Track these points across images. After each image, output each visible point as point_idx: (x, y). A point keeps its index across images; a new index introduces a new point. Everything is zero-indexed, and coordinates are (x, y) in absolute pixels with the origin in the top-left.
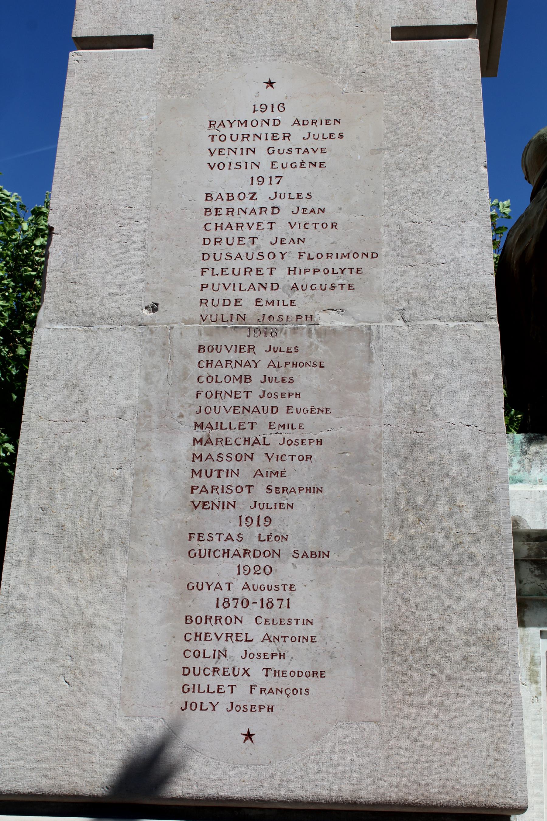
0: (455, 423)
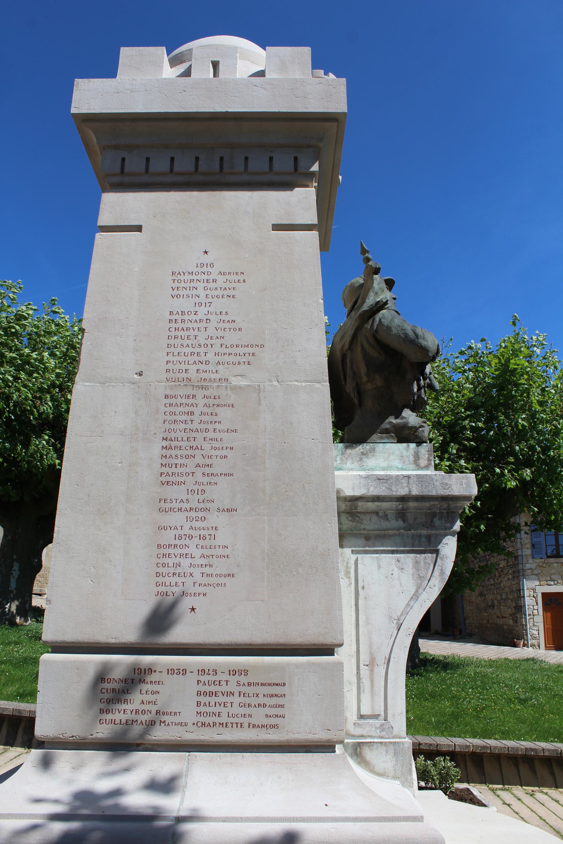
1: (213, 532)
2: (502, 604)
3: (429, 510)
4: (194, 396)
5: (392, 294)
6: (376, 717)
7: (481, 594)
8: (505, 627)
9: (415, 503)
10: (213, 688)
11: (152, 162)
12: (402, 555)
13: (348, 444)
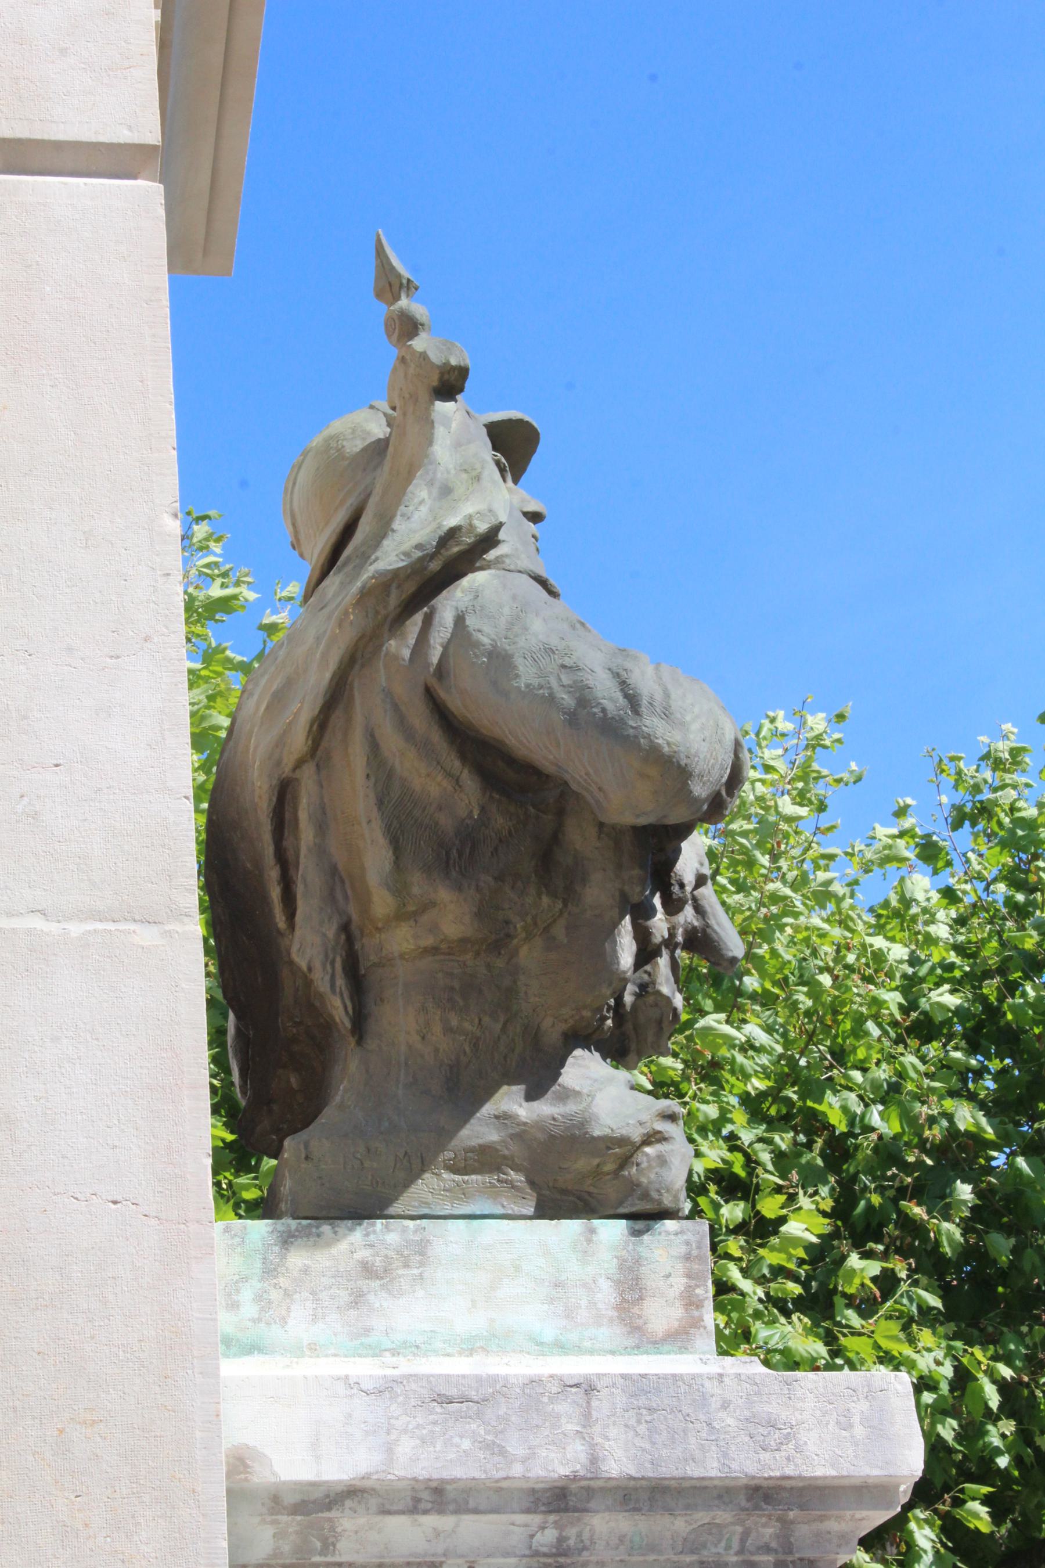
0: (78, 1196)
3: (692, 1552)
5: (523, 494)
9: (621, 1516)
13: (293, 1224)
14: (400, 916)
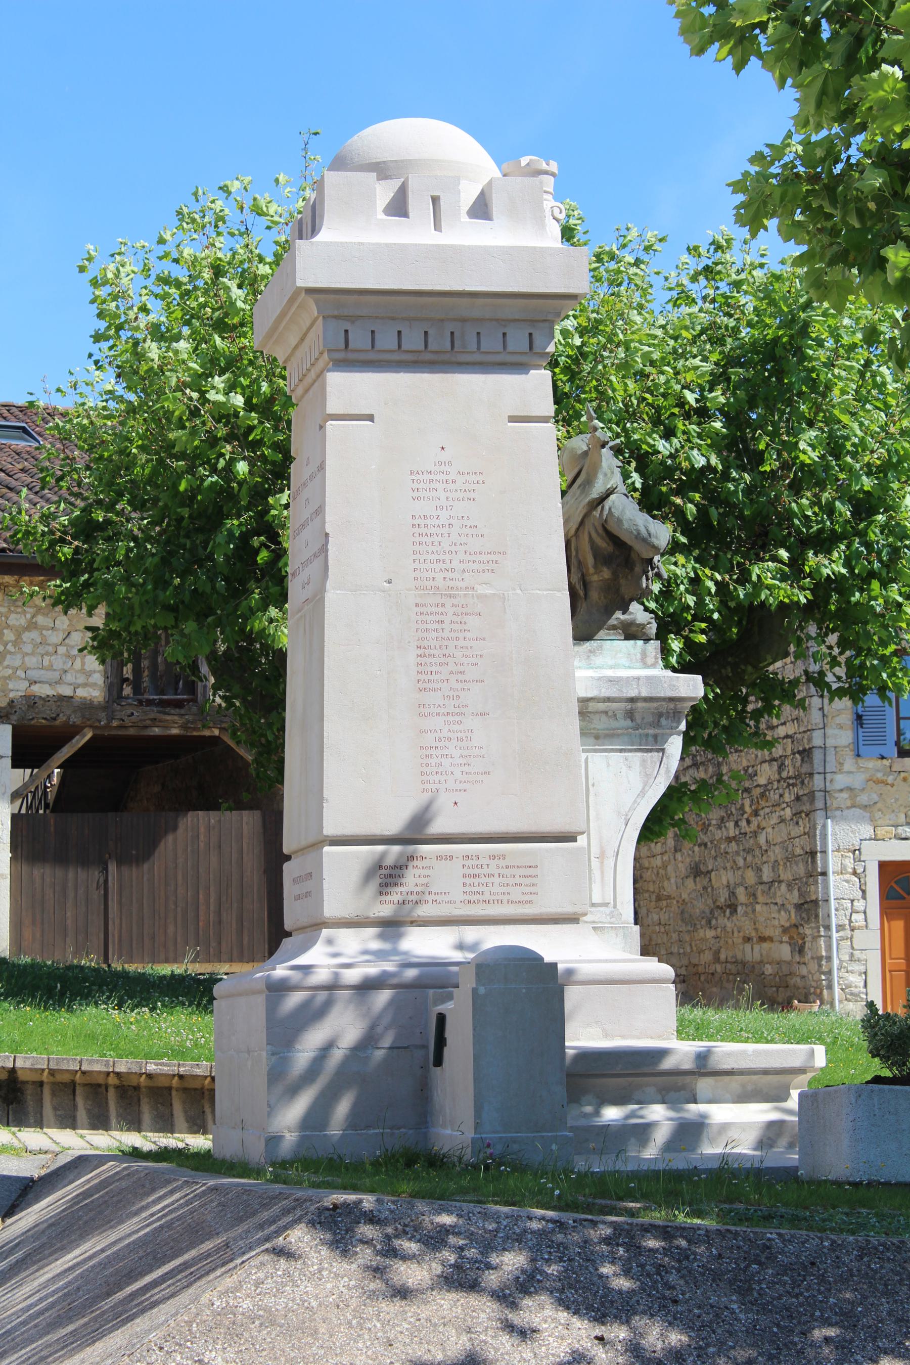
1: (469, 735)
2: (761, 899)
4: (443, 605)
6: (606, 905)
7: (697, 871)
8: (769, 970)
10: (476, 871)
11: (377, 335)
12: (630, 754)
14: (595, 573)
